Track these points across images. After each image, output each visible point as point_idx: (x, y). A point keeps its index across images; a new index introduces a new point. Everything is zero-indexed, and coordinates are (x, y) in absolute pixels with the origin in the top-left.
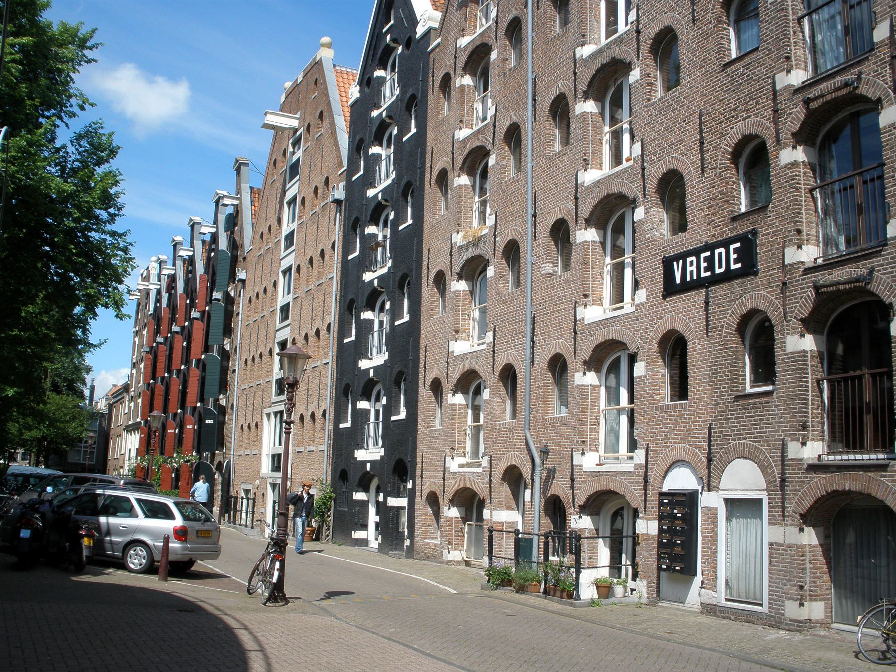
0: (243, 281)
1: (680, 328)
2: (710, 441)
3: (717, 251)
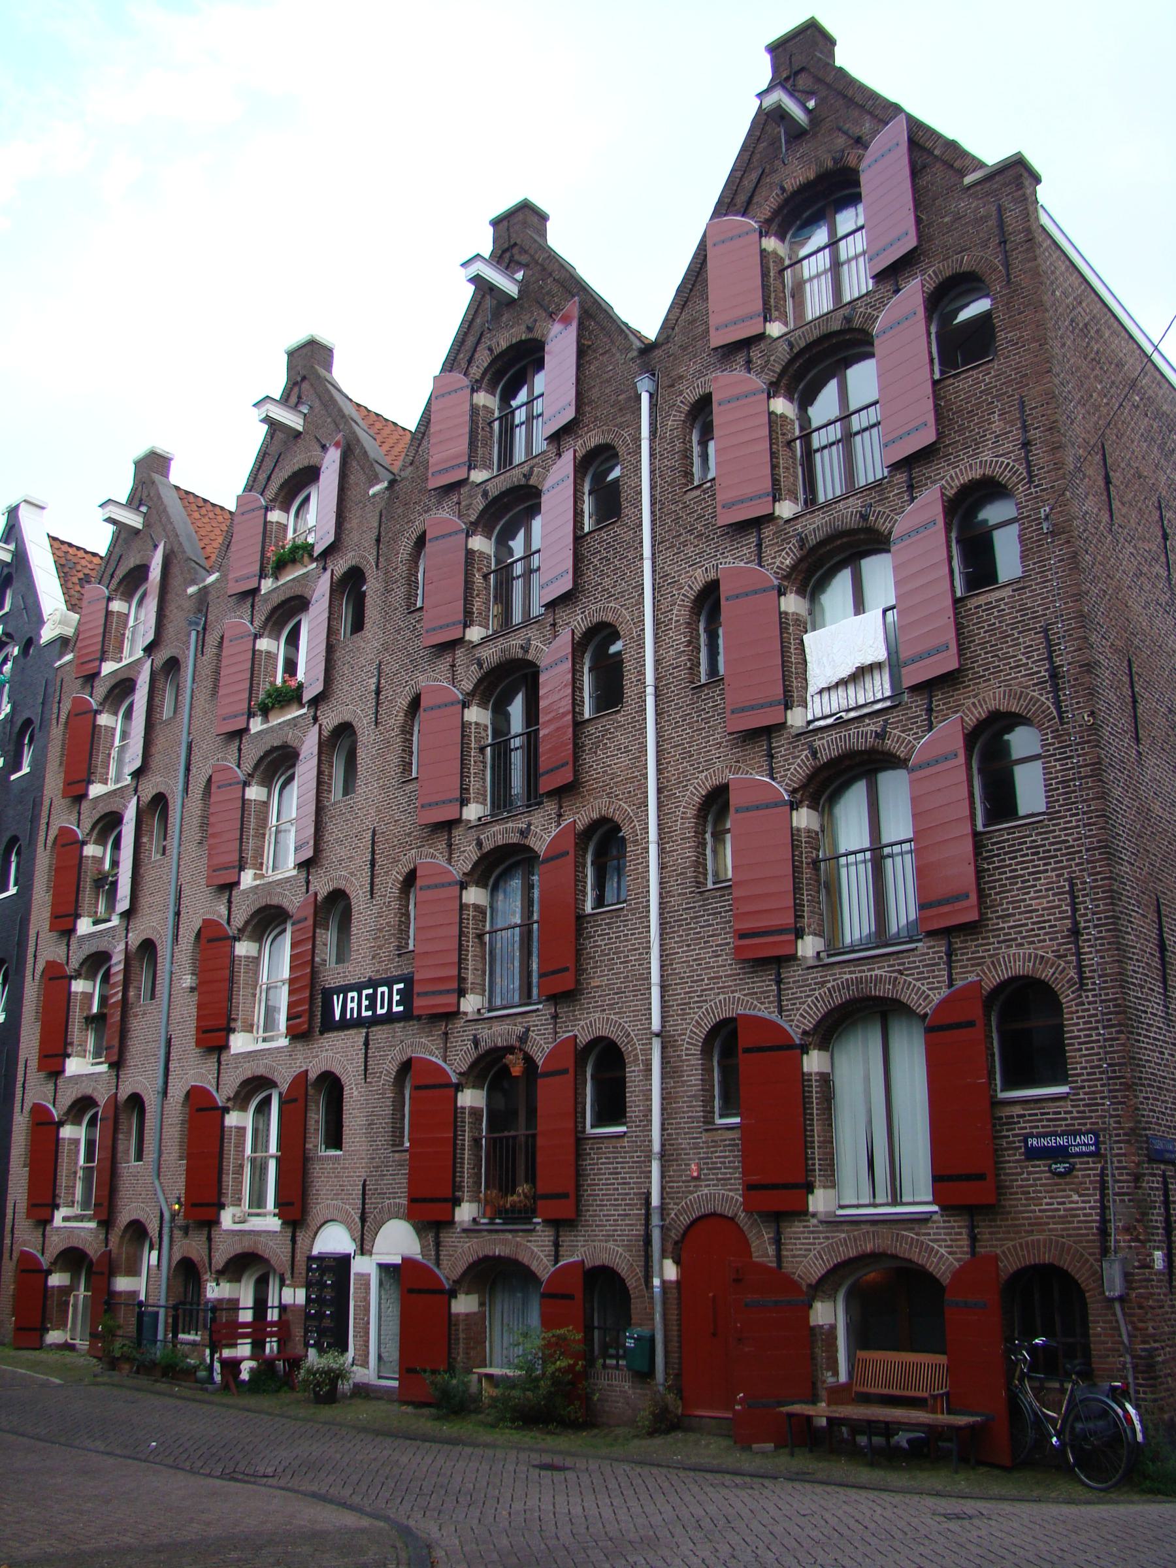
1: (337, 1070)
2: (364, 1199)
3: (380, 990)
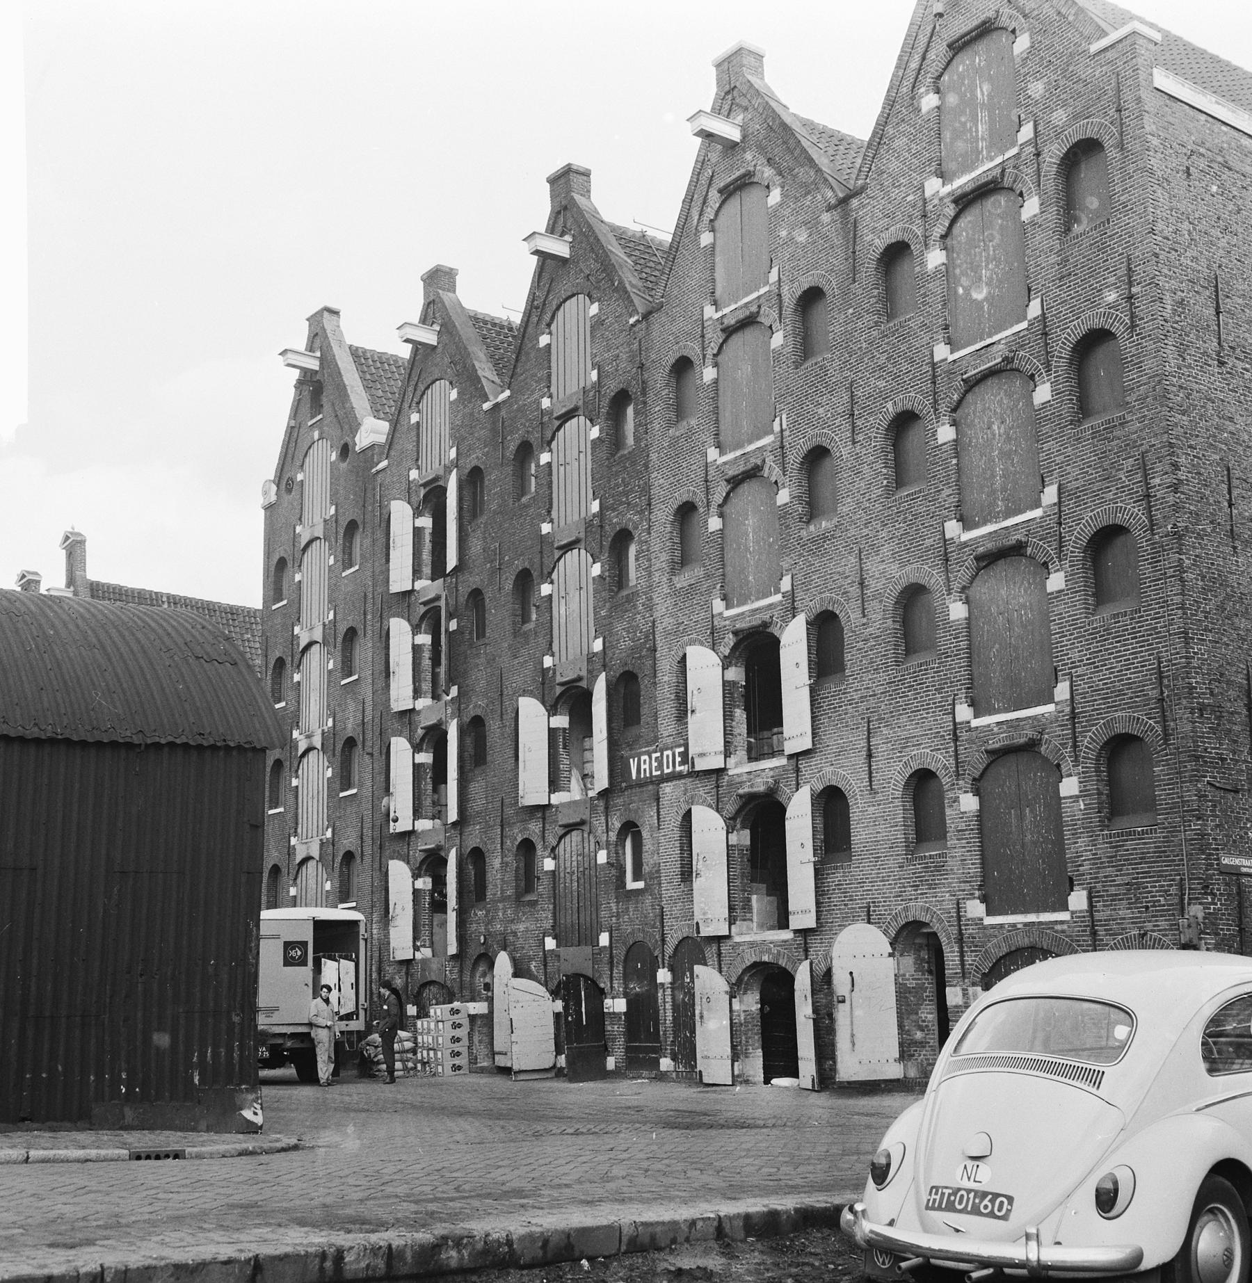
0: (864, 1211)
